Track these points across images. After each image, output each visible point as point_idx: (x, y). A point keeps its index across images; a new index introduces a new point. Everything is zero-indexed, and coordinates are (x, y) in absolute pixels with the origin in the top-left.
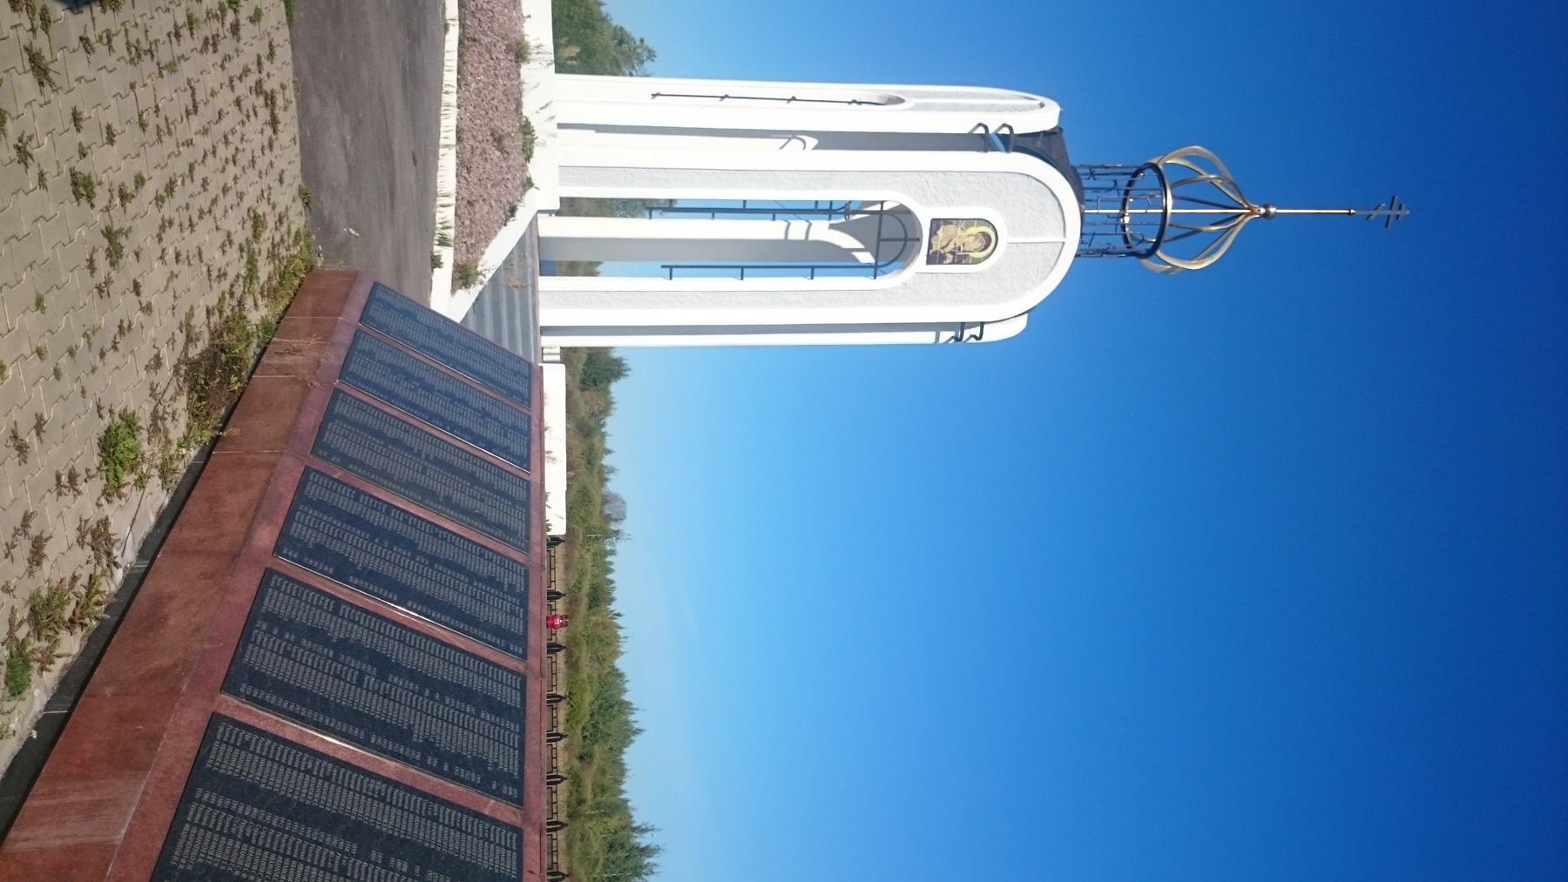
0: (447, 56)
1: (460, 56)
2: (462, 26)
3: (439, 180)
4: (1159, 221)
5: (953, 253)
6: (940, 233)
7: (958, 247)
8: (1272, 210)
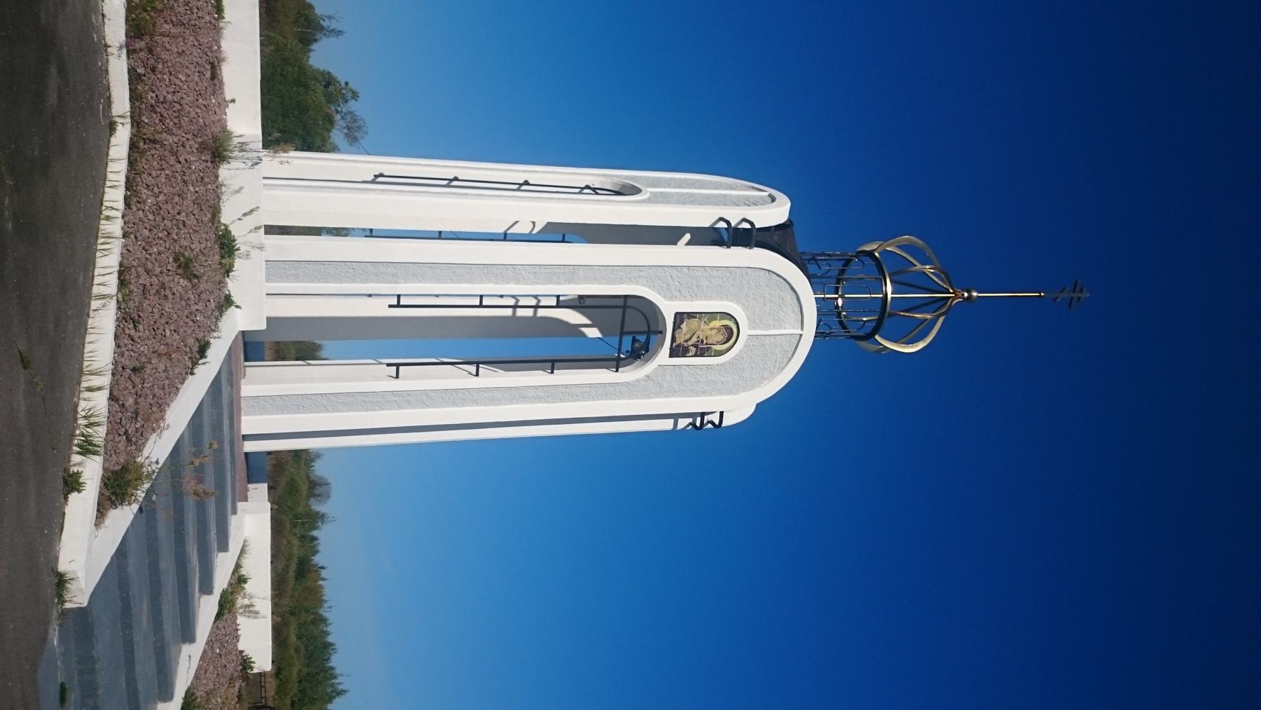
0: (112, 167)
1: (132, 163)
2: (136, 122)
3: (88, 348)
4: (878, 308)
5: (695, 346)
6: (684, 326)
7: (702, 339)
8: (975, 294)
